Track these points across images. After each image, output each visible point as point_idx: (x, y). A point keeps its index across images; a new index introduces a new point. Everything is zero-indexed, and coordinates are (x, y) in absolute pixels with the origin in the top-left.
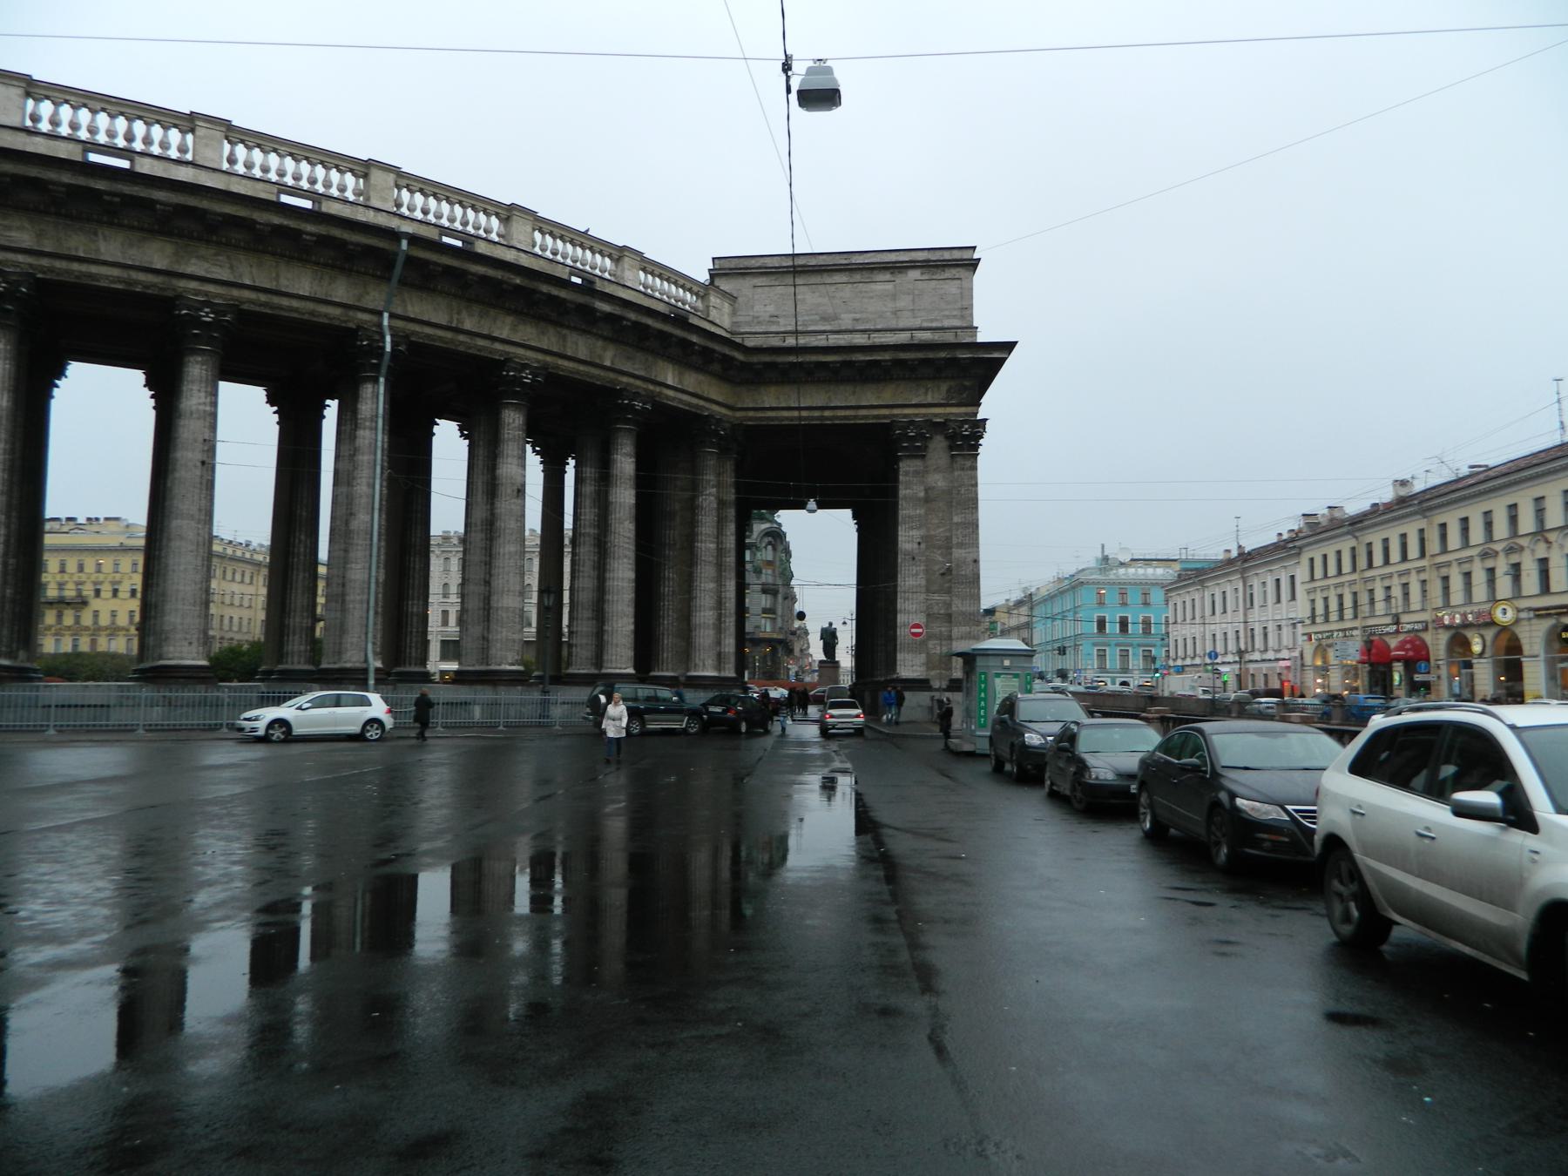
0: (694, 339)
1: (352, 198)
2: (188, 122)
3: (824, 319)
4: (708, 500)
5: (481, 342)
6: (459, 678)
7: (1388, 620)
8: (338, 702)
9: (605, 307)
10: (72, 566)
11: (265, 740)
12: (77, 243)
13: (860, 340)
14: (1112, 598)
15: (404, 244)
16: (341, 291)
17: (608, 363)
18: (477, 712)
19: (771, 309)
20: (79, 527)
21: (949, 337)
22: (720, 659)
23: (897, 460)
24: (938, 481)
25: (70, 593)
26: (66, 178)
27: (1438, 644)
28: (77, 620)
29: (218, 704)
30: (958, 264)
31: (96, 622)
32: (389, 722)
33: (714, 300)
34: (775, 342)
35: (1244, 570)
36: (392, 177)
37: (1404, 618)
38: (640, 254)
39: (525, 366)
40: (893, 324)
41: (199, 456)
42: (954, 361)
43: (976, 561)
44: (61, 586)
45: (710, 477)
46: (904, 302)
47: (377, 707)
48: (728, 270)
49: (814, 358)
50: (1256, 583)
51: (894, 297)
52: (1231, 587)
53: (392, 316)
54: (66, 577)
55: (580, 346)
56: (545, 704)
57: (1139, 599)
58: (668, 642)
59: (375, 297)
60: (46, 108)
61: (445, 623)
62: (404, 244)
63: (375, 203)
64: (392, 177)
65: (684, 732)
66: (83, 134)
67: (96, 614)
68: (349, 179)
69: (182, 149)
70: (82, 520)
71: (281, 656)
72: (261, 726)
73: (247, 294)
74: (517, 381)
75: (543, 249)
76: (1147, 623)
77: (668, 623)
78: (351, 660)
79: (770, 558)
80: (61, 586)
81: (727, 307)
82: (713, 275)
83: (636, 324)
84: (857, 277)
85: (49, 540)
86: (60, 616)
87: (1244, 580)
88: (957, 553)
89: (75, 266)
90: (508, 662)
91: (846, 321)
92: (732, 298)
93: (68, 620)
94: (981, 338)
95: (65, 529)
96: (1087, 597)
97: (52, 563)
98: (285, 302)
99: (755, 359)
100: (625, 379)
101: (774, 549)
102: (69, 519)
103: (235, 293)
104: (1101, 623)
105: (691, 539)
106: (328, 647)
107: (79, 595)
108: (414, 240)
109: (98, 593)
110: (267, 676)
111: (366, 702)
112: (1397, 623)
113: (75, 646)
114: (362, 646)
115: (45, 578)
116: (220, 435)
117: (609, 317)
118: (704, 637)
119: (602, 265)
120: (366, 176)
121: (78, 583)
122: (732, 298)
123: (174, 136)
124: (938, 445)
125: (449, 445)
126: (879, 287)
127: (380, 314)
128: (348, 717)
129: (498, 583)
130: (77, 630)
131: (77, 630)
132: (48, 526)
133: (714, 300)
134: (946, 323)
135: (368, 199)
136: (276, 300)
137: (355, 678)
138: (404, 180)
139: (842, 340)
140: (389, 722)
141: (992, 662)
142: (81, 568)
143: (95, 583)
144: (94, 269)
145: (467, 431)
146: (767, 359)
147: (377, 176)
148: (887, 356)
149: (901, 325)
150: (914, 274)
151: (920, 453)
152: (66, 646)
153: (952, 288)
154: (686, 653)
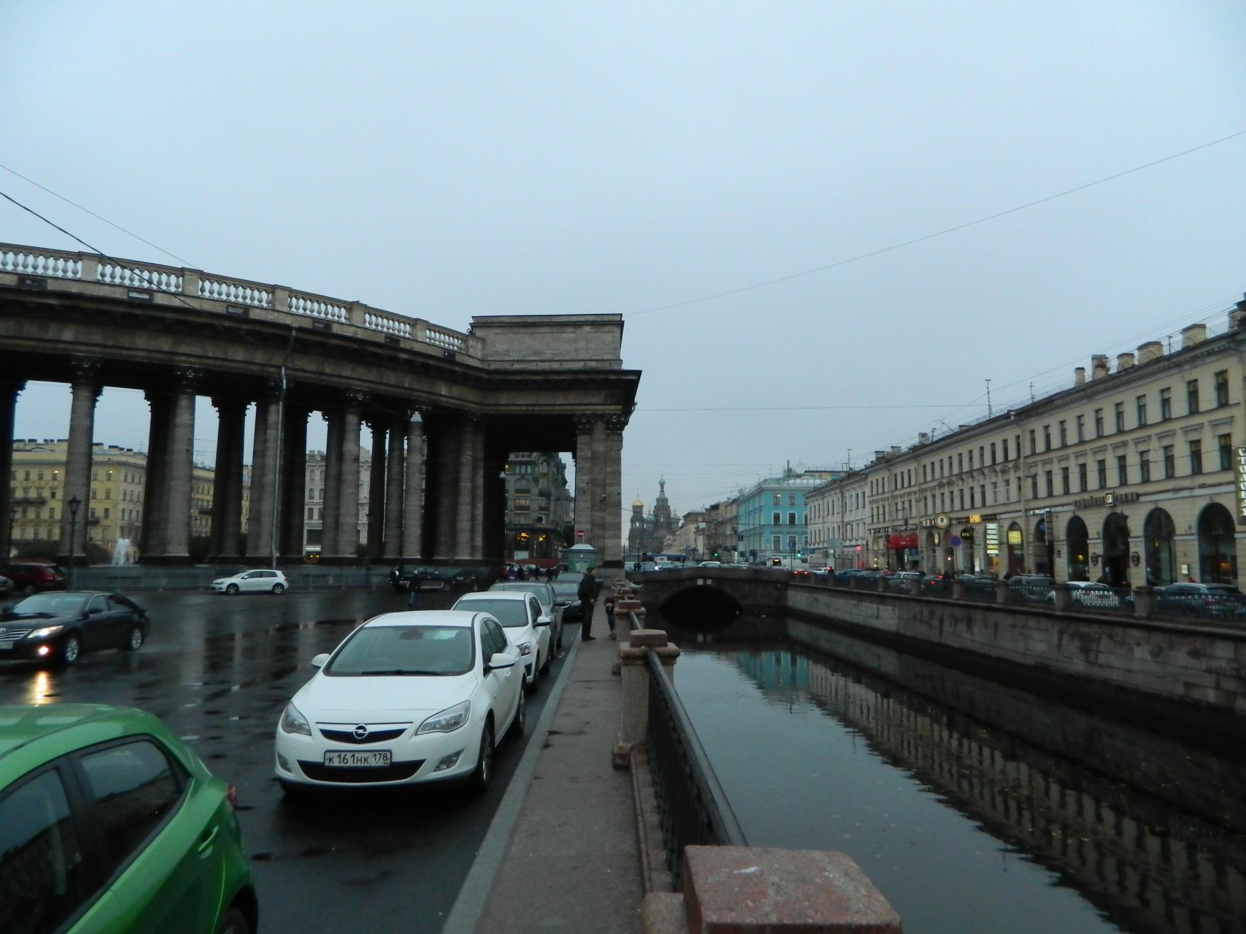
0: (457, 369)
1: (265, 305)
2: (180, 272)
3: (536, 353)
4: (467, 457)
5: (335, 379)
6: (322, 562)
7: (902, 523)
8: (261, 575)
9: (404, 356)
10: (34, 475)
11: (226, 593)
12: (125, 340)
13: (556, 366)
14: (784, 499)
15: (294, 333)
16: (259, 357)
17: (406, 385)
18: (331, 581)
19: (505, 347)
20: (39, 446)
21: (606, 366)
22: (473, 550)
23: (575, 436)
24: (599, 447)
25: (33, 494)
26: (121, 309)
27: (922, 536)
28: (38, 516)
29: (195, 577)
30: (615, 323)
31: (52, 516)
32: (286, 585)
33: (471, 342)
34: (507, 366)
35: (842, 487)
36: (287, 293)
37: (910, 522)
38: (426, 322)
39: (358, 391)
40: (575, 357)
41: (186, 447)
42: (607, 381)
43: (619, 494)
44: (26, 490)
45: (468, 445)
46: (581, 344)
47: (280, 577)
48: (481, 323)
49: (528, 377)
50: (847, 495)
51: (575, 341)
52: (834, 498)
53: (287, 368)
54: (30, 484)
55: (391, 377)
56: (368, 576)
57: (788, 501)
58: (443, 539)
59: (277, 360)
60: (108, 269)
61: (311, 517)
62: (294, 333)
63: (278, 308)
64: (287, 293)
65: (442, 590)
66: (127, 282)
67: (52, 510)
68: (264, 295)
69: (177, 286)
70: (40, 441)
71: (220, 548)
72: (224, 587)
73: (210, 361)
74: (355, 399)
75: (370, 324)
76: (792, 517)
77: (443, 529)
78: (263, 552)
79: (545, 471)
80: (26, 490)
81: (479, 346)
82: (473, 326)
83: (422, 364)
84: (555, 329)
85: (16, 456)
86: (25, 512)
87: (842, 493)
88: (609, 489)
89: (124, 352)
90: (348, 553)
91: (548, 356)
92: (483, 340)
93: (31, 515)
94: (625, 367)
95: (28, 448)
96: (766, 500)
97: (19, 473)
98: (230, 364)
99: (494, 377)
100: (416, 394)
101: (548, 464)
102: (31, 441)
103: (205, 361)
104: (777, 518)
105: (457, 480)
106: (250, 542)
107: (40, 497)
108: (300, 329)
109: (53, 495)
110: (212, 561)
111: (274, 575)
112: (906, 524)
113: (36, 534)
114: (269, 546)
115: (12, 484)
116: (196, 436)
117: (406, 361)
118: (463, 537)
119: (403, 330)
120: (273, 293)
121: (38, 488)
122: (483, 340)
123: (173, 279)
124: (600, 428)
125: (317, 429)
126: (569, 335)
127: (280, 368)
128: (266, 583)
129: (343, 510)
130: (38, 522)
131: (38, 522)
132: (15, 446)
133: (471, 342)
134: (605, 357)
135: (274, 305)
136: (225, 363)
137: (264, 562)
138: (293, 293)
139: (546, 366)
140: (286, 585)
141: (575, 555)
142: (41, 477)
143: (51, 488)
144: (133, 353)
145: (328, 415)
146: (501, 377)
147: (279, 293)
148: (569, 377)
149: (580, 357)
150: (588, 329)
151: (589, 432)
152: (29, 535)
153: (608, 337)
154: (453, 546)
